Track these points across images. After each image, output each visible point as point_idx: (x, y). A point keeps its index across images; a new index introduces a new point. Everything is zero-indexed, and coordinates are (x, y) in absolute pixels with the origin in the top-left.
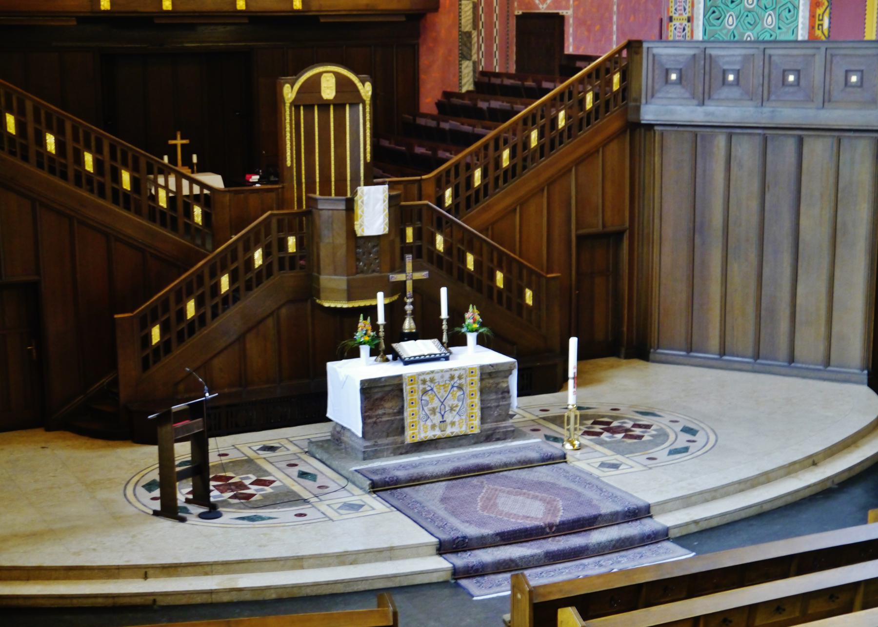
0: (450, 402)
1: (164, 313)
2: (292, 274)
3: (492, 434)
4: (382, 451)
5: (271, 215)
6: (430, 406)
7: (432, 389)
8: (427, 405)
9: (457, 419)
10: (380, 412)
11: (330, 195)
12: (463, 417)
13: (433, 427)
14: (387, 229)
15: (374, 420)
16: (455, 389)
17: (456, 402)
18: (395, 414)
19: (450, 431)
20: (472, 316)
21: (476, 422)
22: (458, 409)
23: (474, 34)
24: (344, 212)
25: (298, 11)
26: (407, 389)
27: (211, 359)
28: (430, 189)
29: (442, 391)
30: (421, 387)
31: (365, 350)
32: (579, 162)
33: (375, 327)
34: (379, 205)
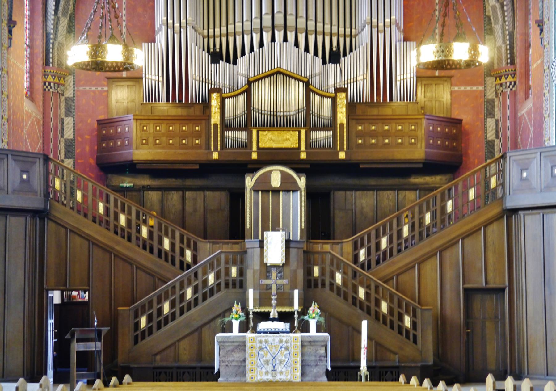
0: (280, 357)
1: (149, 309)
2: (234, 290)
5: (221, 252)
6: (264, 358)
7: (266, 348)
9: (284, 370)
13: (267, 373)
14: (284, 260)
15: (226, 363)
16: (283, 349)
17: (283, 358)
18: (241, 362)
19: (278, 377)
20: (314, 308)
21: (298, 374)
22: (285, 363)
23: (497, 141)
24: (259, 249)
26: (248, 345)
27: (179, 341)
28: (348, 247)
29: (274, 350)
30: (258, 345)
32: (465, 236)
33: (245, 309)
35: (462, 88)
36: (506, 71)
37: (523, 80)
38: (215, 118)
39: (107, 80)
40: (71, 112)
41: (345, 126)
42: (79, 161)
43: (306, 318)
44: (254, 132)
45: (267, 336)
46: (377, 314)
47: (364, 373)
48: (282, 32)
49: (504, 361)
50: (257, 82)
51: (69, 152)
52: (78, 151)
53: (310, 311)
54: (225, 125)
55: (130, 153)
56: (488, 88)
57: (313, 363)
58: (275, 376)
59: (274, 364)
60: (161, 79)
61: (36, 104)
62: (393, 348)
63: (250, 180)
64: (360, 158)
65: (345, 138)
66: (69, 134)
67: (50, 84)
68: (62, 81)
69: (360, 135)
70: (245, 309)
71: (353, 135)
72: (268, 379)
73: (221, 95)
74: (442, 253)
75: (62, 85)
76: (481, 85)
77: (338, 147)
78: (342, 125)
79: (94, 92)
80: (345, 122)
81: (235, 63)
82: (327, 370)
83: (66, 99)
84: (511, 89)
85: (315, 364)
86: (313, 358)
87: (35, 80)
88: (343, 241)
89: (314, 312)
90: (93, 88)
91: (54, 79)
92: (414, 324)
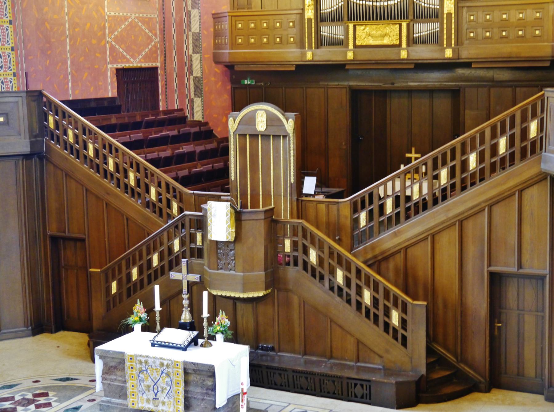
0: (161, 384)
6: (145, 383)
7: (146, 370)
9: (166, 400)
10: (113, 377)
11: (259, 207)
16: (164, 375)
17: (165, 386)
25: (449, 59)
26: (128, 364)
28: (346, 211)
29: (155, 374)
31: (138, 327)
32: (492, 204)
33: (150, 310)
38: (310, 13)
40: (196, 3)
41: (453, 16)
42: (206, 56)
44: (351, 26)
46: (359, 304)
49: (542, 374)
51: (196, 46)
52: (204, 45)
54: (321, 18)
57: (200, 397)
58: (157, 406)
59: (156, 392)
62: (376, 350)
66: (196, 27)
70: (150, 310)
71: (465, 26)
72: (149, 408)
74: (492, 207)
80: (453, 11)
85: (201, 397)
92: (404, 322)
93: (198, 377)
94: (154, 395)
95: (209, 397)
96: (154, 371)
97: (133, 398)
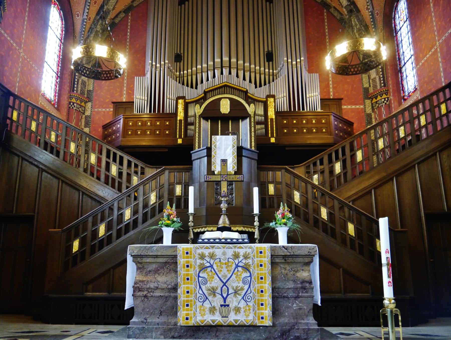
0: (234, 283)
3: (289, 331)
4: (150, 331)
6: (208, 285)
7: (211, 266)
8: (206, 283)
9: (242, 304)
12: (251, 304)
13: (212, 310)
14: (236, 168)
15: (145, 293)
16: (240, 269)
17: (241, 284)
19: (233, 318)
21: (267, 312)
26: (181, 261)
29: (224, 270)
30: (199, 262)
34: (229, 149)
35: (349, 107)
36: (381, 91)
37: (396, 94)
38: (181, 115)
39: (112, 104)
43: (272, 224)
45: (213, 247)
47: (392, 311)
48: (220, 70)
50: (219, 90)
53: (278, 215)
55: (74, 61)
56: (367, 106)
57: (291, 294)
59: (225, 295)
60: (146, 98)
61: (61, 113)
63: (199, 107)
64: (286, 143)
65: (274, 129)
67: (73, 104)
68: (83, 104)
69: (285, 126)
72: (213, 321)
73: (185, 101)
75: (83, 106)
76: (361, 104)
77: (270, 135)
78: (272, 119)
79: (104, 112)
80: (274, 117)
81: (196, 88)
82: (315, 305)
83: (86, 117)
84: (386, 104)
85: (294, 295)
86: (291, 285)
87: (62, 98)
88: (295, 166)
89: (283, 217)
90: (104, 110)
91: (76, 101)
93: (288, 268)
94: (222, 300)
95: (307, 292)
96: (224, 266)
97: (187, 310)
